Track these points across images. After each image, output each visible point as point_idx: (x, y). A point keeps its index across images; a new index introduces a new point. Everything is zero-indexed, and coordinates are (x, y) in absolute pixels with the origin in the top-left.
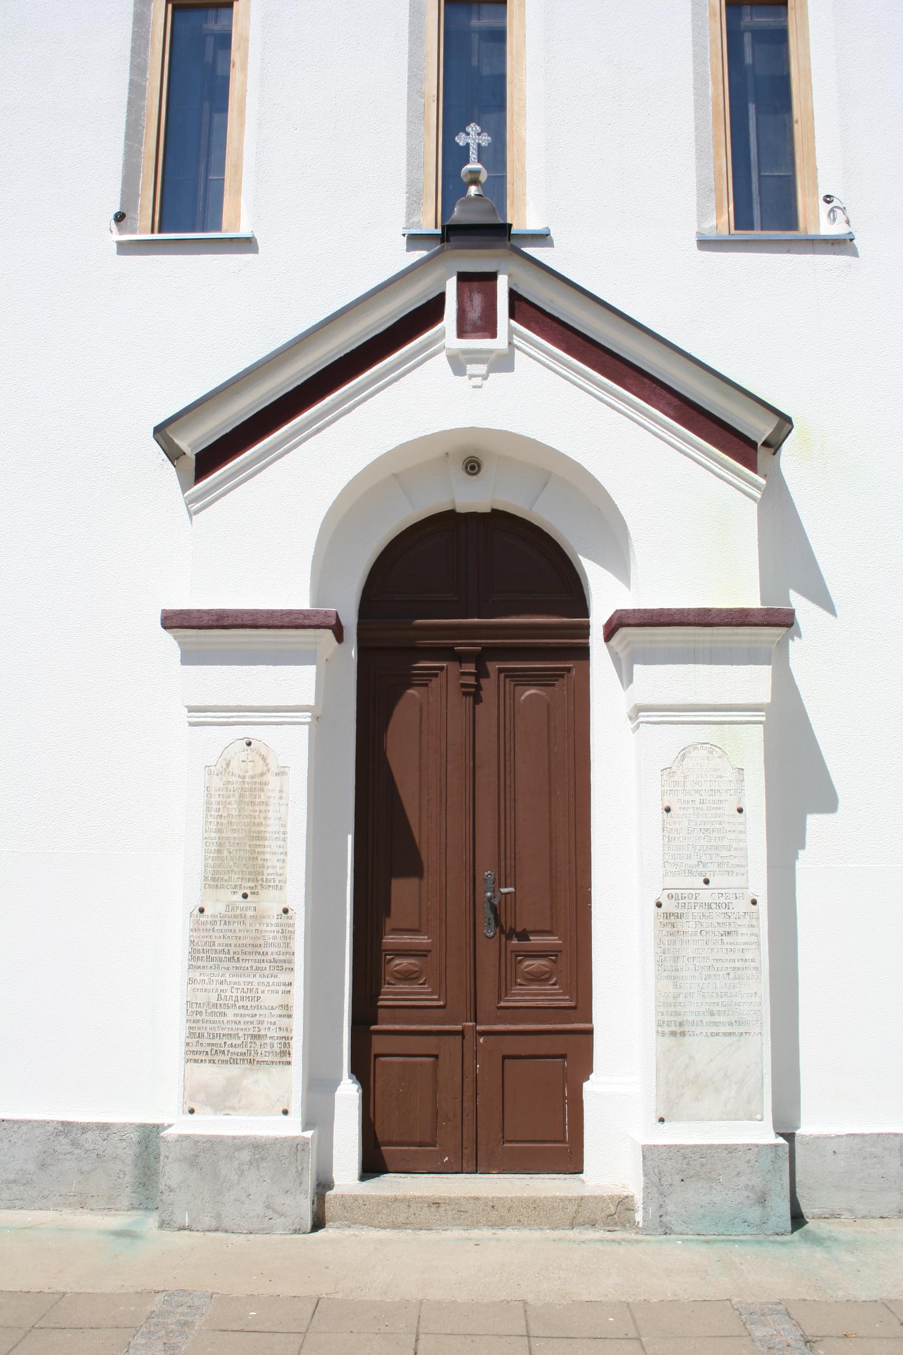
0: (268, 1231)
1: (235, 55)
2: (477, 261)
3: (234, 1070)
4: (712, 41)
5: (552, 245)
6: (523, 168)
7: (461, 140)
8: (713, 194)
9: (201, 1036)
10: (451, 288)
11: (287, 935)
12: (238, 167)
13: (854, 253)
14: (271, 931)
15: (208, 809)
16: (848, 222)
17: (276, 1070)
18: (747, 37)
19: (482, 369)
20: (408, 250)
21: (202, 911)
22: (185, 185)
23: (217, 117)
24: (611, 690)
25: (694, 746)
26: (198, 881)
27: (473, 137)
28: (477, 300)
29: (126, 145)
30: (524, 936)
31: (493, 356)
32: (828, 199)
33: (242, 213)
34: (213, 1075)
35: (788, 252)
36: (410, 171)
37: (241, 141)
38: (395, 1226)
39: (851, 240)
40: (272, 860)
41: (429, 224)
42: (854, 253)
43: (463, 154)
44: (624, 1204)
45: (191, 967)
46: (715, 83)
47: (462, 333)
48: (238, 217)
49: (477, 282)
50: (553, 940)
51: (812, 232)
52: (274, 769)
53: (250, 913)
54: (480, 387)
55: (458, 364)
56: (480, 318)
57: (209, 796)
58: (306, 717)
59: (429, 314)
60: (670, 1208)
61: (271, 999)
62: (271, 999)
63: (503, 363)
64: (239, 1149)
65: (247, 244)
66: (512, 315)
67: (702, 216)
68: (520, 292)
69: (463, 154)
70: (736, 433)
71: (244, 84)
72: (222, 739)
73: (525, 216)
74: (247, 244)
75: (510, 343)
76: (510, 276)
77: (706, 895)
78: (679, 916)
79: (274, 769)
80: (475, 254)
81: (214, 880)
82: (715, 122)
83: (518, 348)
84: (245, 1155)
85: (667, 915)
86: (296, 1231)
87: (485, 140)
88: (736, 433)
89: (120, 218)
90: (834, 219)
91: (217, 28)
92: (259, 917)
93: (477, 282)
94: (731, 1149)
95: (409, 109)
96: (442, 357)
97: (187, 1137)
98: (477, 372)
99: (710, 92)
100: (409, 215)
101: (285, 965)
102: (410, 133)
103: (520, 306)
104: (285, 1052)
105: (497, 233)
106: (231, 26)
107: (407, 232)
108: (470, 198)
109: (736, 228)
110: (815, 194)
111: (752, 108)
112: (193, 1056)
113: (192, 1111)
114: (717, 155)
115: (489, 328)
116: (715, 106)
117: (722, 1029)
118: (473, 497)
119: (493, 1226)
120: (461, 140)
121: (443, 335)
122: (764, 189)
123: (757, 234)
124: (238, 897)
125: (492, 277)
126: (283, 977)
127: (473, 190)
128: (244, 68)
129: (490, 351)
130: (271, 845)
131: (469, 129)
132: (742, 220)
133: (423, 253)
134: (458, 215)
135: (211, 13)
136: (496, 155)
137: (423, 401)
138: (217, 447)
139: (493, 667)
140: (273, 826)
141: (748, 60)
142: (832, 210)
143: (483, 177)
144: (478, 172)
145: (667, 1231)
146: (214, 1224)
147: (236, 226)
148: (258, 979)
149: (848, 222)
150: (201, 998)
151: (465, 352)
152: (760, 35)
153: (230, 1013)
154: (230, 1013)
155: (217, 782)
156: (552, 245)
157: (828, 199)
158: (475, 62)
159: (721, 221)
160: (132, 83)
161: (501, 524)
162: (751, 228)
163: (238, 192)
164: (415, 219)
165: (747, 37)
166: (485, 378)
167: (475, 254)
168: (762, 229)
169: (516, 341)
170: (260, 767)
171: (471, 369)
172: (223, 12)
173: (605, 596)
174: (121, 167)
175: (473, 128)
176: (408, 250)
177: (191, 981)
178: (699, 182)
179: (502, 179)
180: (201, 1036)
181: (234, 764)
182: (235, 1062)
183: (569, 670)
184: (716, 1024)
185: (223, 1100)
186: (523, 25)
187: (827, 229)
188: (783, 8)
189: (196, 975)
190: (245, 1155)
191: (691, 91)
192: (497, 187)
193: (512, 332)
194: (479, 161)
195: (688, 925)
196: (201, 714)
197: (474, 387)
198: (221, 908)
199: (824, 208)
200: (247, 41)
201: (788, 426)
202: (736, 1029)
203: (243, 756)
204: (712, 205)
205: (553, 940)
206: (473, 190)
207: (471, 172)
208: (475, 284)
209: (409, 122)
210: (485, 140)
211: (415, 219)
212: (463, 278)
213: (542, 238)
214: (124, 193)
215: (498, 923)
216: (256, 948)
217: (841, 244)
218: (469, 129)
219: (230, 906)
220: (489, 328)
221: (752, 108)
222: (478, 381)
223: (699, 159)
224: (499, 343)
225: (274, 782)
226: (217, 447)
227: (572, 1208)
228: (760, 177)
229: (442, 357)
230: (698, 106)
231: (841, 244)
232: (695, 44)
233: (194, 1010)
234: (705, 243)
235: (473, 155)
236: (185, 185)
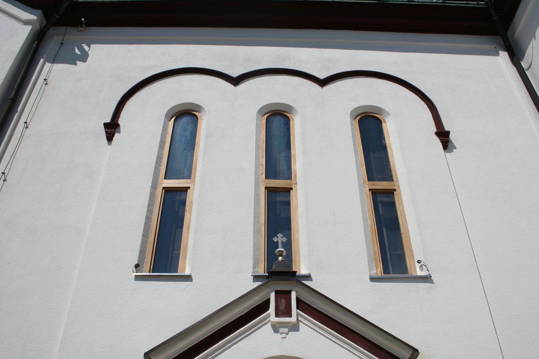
1: (187, 208)
2: (283, 286)
4: (368, 205)
5: (312, 280)
6: (299, 251)
7: (275, 239)
8: (374, 261)
12: (186, 248)
13: (432, 282)
16: (428, 270)
18: (380, 205)
19: (286, 330)
20: (254, 282)
22: (164, 256)
23: (178, 230)
27: (280, 238)
28: (283, 301)
29: (142, 239)
31: (290, 325)
32: (419, 262)
33: (187, 267)
35: (406, 282)
36: (254, 251)
37: (188, 239)
39: (430, 277)
41: (262, 271)
42: (432, 282)
43: (276, 245)
46: (370, 220)
47: (277, 315)
48: (185, 267)
49: (283, 295)
51: (414, 274)
54: (285, 338)
55: (276, 328)
56: (285, 309)
59: (264, 307)
63: (295, 328)
65: (188, 278)
66: (298, 308)
67: (370, 269)
68: (301, 298)
69: (276, 245)
71: (190, 220)
73: (302, 268)
74: (188, 278)
75: (297, 319)
76: (296, 292)
80: (282, 283)
82: (372, 234)
83: (301, 322)
87: (285, 239)
89: (137, 266)
90: (422, 269)
91: (181, 198)
93: (283, 295)
95: (254, 228)
96: (269, 324)
98: (284, 332)
99: (369, 223)
100: (254, 268)
102: (254, 237)
103: (302, 305)
105: (290, 275)
106: (186, 198)
107: (254, 274)
108: (279, 261)
109: (384, 273)
110: (414, 260)
111: (384, 229)
114: (374, 246)
115: (289, 314)
116: (371, 228)
120: (275, 239)
121: (269, 316)
123: (391, 275)
125: (289, 292)
127: (280, 258)
128: (190, 212)
129: (289, 323)
131: (278, 236)
132: (386, 270)
133: (260, 283)
134: (275, 268)
135: (179, 193)
136: (288, 245)
141: (381, 212)
142: (421, 266)
143: (284, 253)
144: (282, 251)
147: (184, 271)
149: (428, 270)
152: (384, 204)
156: (312, 280)
157: (419, 262)
158: (278, 212)
159: (378, 271)
160: (147, 216)
162: (389, 273)
163: (185, 258)
164: (256, 270)
165: (380, 205)
166: (287, 334)
167: (282, 283)
168: (393, 274)
169: (300, 318)
171: (281, 330)
172: (183, 193)
174: (139, 247)
175: (280, 235)
176: (254, 282)
178: (368, 256)
179: (291, 255)
186: (297, 199)
187: (419, 273)
188: (391, 195)
191: (362, 223)
192: (289, 257)
193: (298, 315)
194: (283, 248)
197: (283, 338)
199: (417, 265)
200: (192, 203)
201: (417, 353)
204: (374, 264)
206: (280, 258)
207: (279, 251)
208: (282, 295)
209: (254, 233)
210: (285, 239)
211: (256, 270)
212: (277, 293)
213: (308, 277)
214: (139, 257)
217: (427, 279)
218: (278, 236)
220: (289, 314)
221: (384, 229)
222: (284, 335)
223: (367, 247)
228: (390, 254)
229: (269, 324)
230: (365, 228)
231: (427, 279)
232: (362, 206)
234: (373, 279)
235: (280, 245)
236: (164, 256)
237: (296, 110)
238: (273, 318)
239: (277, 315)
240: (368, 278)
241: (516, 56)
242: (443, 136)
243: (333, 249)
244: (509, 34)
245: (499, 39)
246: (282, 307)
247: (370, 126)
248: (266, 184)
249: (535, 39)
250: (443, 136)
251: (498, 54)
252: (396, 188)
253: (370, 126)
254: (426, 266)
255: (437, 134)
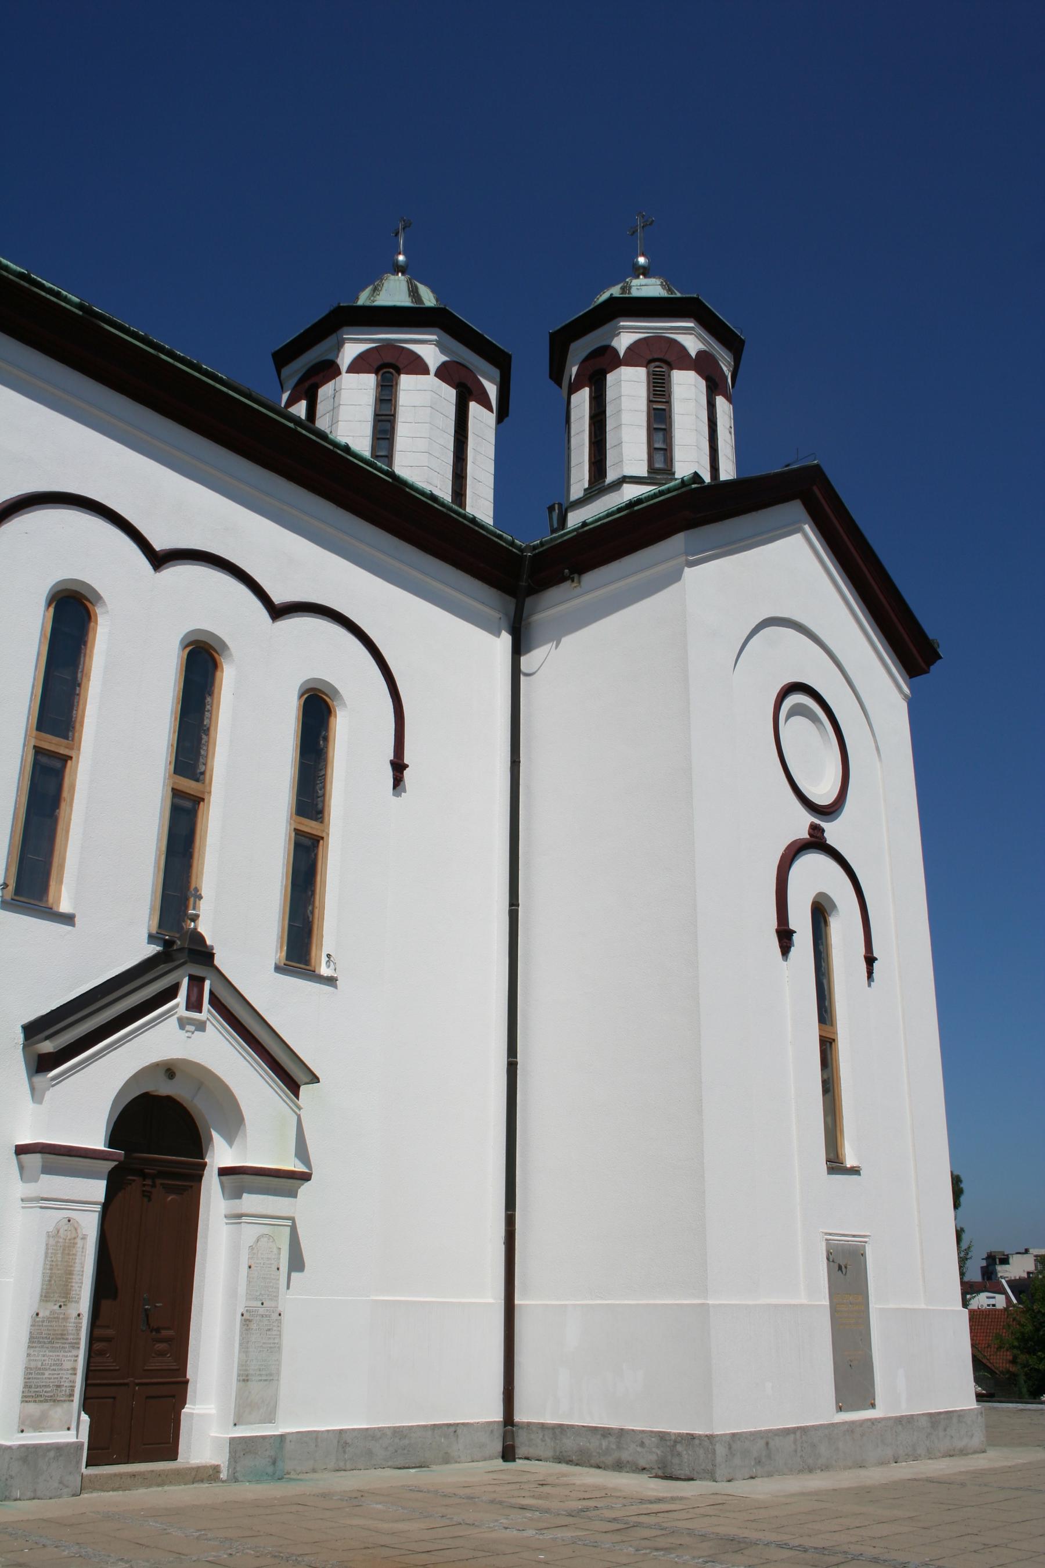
0: (60, 1497)
2: (198, 971)
3: (45, 1406)
9: (30, 1387)
10: (185, 982)
11: (78, 1329)
12: (62, 867)
13: (336, 987)
14: (71, 1326)
15: (46, 1257)
17: (65, 1405)
19: (192, 1028)
21: (37, 1314)
24: (214, 1202)
25: (262, 1236)
26: (37, 1297)
28: (195, 990)
30: (158, 1330)
34: (34, 1409)
38: (113, 1490)
40: (76, 1286)
42: (336, 987)
44: (216, 1469)
45: (29, 1347)
47: (188, 1009)
49: (197, 982)
50: (171, 1333)
52: (80, 1236)
53: (62, 1316)
55: (182, 1023)
57: (47, 1249)
58: (99, 1208)
60: (238, 1469)
61: (68, 1365)
62: (68, 1365)
63: (201, 1026)
64: (49, 1450)
65: (68, 919)
70: (289, 1074)
72: (55, 1217)
74: (68, 919)
77: (261, 1311)
78: (250, 1321)
79: (80, 1236)
80: (180, 955)
81: (45, 1297)
84: (52, 1454)
85: (246, 1320)
86: (74, 1495)
88: (289, 1074)
92: (66, 1319)
93: (197, 982)
94: (264, 1437)
97: (23, 1445)
101: (75, 1346)
103: (215, 1001)
104: (72, 1395)
112: (26, 1399)
113: (22, 1431)
115: (199, 1008)
117: (264, 1378)
118: (164, 1088)
119: (159, 1485)
122: (299, 949)
124: (57, 1307)
125: (202, 980)
126: (74, 1353)
129: (873, 1422)
130: (76, 1278)
137: (163, 1039)
138: (57, 1040)
139: (159, 1181)
140: (77, 1268)
145: (236, 1480)
146: (32, 1495)
148: (62, 1353)
150: (33, 1365)
151: (188, 1019)
153: (47, 1373)
154: (47, 1373)
155: (52, 1241)
161: (170, 1102)
170: (74, 1235)
171: (188, 1027)
173: (222, 1154)
177: (28, 1355)
180: (30, 1387)
181: (61, 1231)
182: (46, 1401)
183: (191, 1187)
184: (261, 1375)
185: (38, 1424)
187: (324, 971)
189: (31, 1351)
190: (52, 1454)
195: (254, 1326)
196: (45, 1202)
198: (47, 1313)
199: (324, 959)
202: (268, 1378)
203: (66, 1228)
205: (171, 1333)
212: (192, 978)
215: (148, 1324)
216: (62, 1336)
217: (331, 981)
219: (52, 1312)
220: (199, 1008)
222: (189, 1034)
224: (203, 1016)
225: (80, 1243)
226: (57, 1040)
227: (193, 1473)
231: (331, 981)
233: (29, 1372)
236: (32, 883)
237: (231, 655)
238: (182, 1011)
239: (188, 1009)
240: (273, 966)
241: (518, 650)
242: (398, 767)
243: (239, 914)
244: (529, 601)
245: (511, 603)
246: (194, 998)
247: (317, 710)
248: (174, 783)
249: (556, 647)
250: (398, 767)
251: (498, 635)
252: (324, 835)
253: (317, 710)
254: (335, 964)
255: (392, 763)
